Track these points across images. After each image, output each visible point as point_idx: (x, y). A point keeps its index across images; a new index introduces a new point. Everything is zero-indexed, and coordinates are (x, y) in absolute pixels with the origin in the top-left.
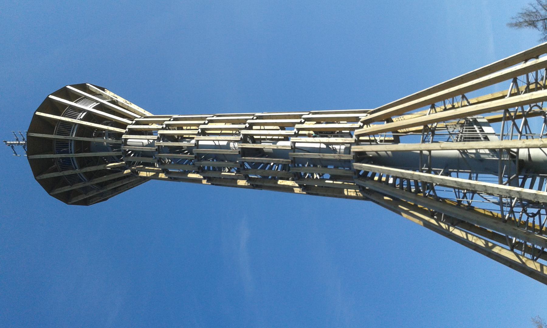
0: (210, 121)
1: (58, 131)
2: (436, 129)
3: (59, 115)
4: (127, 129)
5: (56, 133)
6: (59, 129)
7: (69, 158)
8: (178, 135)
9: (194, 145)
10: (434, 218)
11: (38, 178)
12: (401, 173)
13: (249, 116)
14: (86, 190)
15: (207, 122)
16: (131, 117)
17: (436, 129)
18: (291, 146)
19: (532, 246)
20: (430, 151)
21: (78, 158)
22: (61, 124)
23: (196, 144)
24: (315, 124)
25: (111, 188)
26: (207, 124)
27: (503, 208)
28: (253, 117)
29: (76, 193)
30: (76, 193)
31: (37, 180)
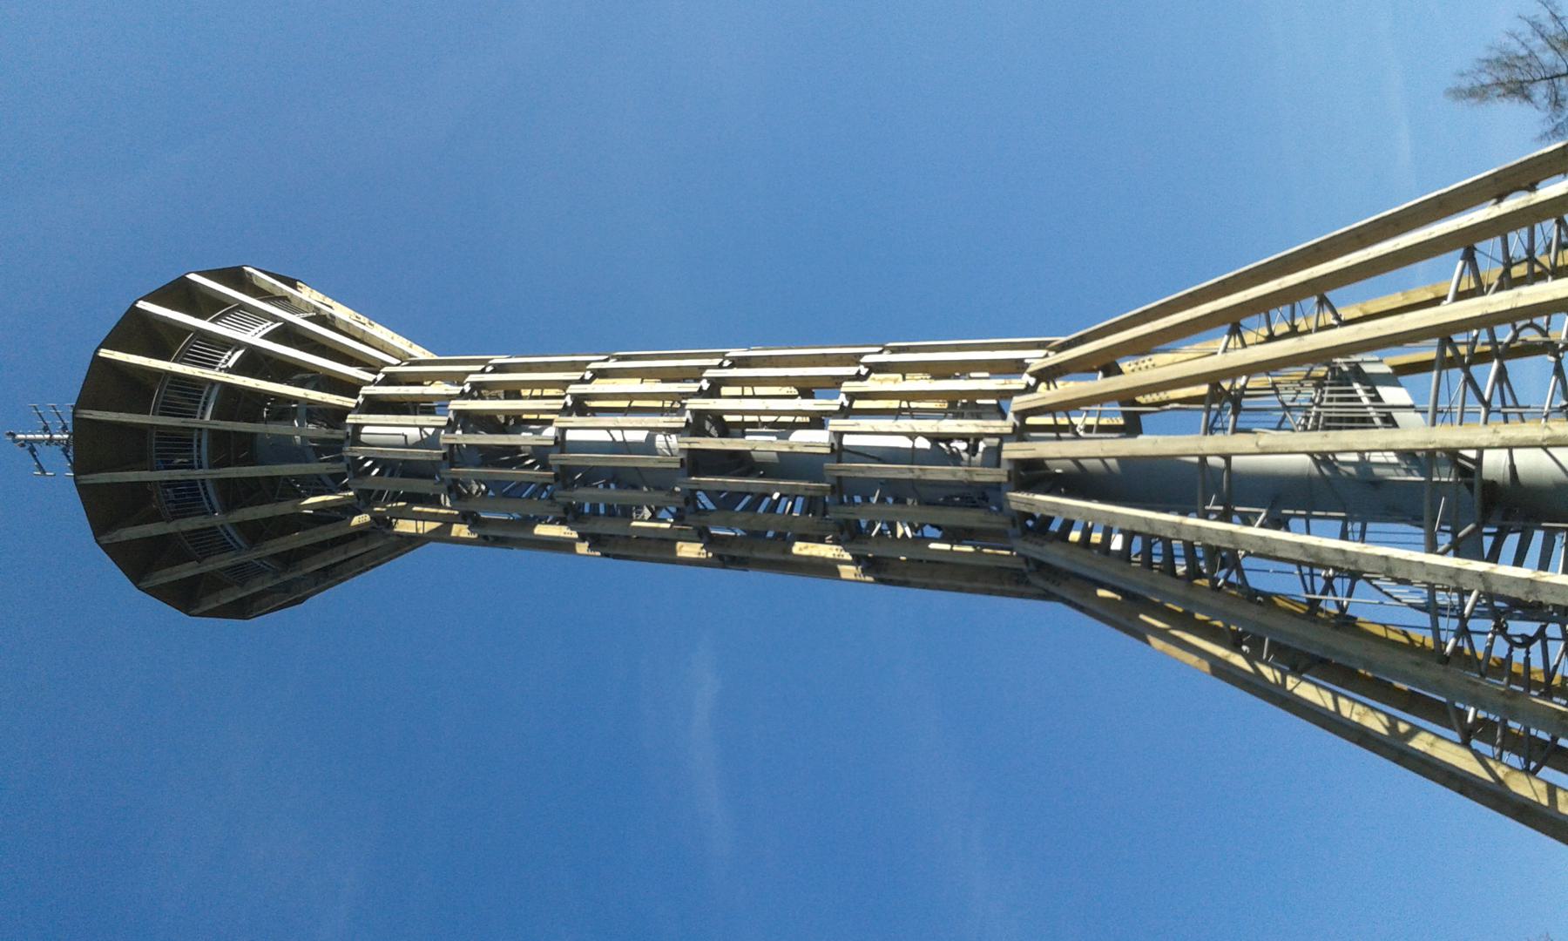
3: (166, 358)
29: (213, 583)
30: (213, 583)
31: (101, 546)
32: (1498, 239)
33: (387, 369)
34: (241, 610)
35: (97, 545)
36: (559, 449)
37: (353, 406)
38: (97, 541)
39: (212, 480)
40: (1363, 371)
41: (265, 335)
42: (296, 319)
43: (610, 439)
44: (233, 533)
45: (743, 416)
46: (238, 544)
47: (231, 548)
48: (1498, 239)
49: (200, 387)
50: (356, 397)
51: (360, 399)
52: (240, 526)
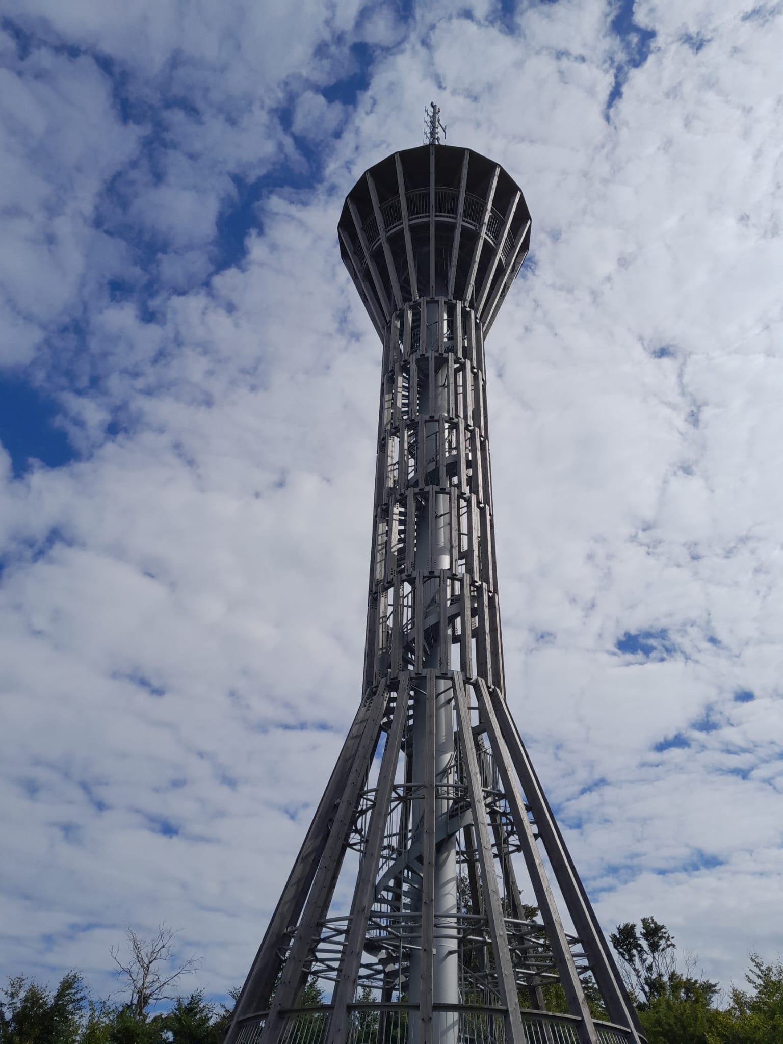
0: (483, 511)
1: (445, 193)
2: (339, 956)
3: (468, 189)
4: (455, 301)
5: (438, 191)
6: (449, 193)
7: (401, 218)
8: (469, 788)
9: (454, 573)
10: (655, 925)
11: (368, 175)
12: (474, 841)
13: (493, 569)
14: (358, 252)
15: (482, 505)
16: (479, 297)
17: (339, 956)
18: (457, 574)
19: (508, 805)
20: (478, 537)
21: (402, 231)
22: (455, 195)
23: (455, 577)
24: (498, 595)
25: (364, 287)
26: (478, 506)
27: (315, 955)
28: (493, 592)
29: (353, 237)
30: (353, 237)
31: (365, 173)
32: (467, 533)
33: (473, 312)
34: (344, 255)
35: (364, 171)
36: (459, 494)
37: (466, 305)
38: (366, 171)
39: (403, 228)
40: (456, 618)
41: (487, 240)
42: (500, 255)
43: (466, 514)
44: (378, 243)
45: (596, 983)
46: (389, 231)
47: (370, 244)
48: (467, 533)
49: (473, 203)
50: (469, 307)
51: (468, 309)
52: (381, 246)
